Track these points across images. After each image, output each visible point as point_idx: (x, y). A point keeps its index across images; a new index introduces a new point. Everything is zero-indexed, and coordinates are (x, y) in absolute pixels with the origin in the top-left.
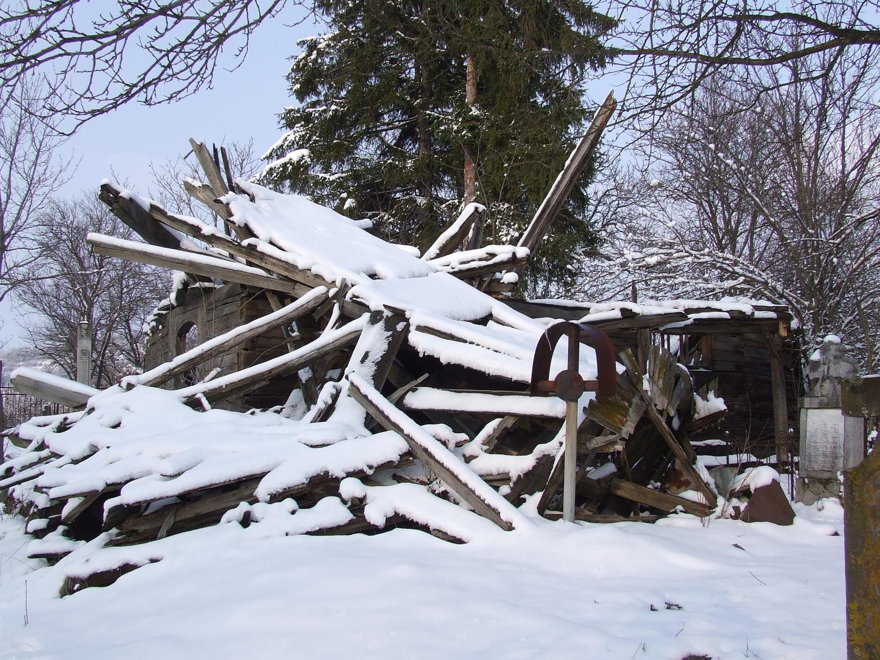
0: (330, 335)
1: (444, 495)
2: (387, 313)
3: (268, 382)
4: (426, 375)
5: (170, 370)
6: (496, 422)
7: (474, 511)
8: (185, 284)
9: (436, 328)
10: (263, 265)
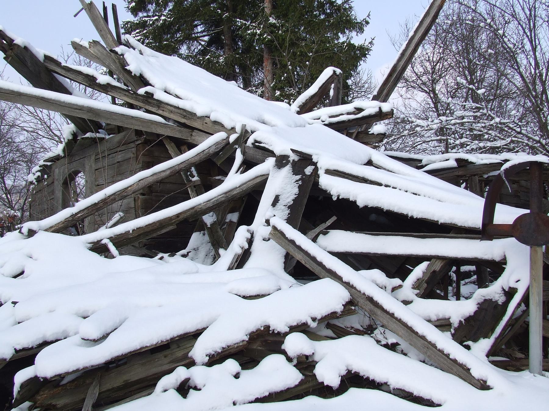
0: (234, 180)
1: (393, 347)
2: (293, 157)
3: (175, 227)
4: (334, 218)
5: (73, 216)
6: (424, 266)
7: (424, 362)
8: (75, 135)
9: (347, 172)
10: (160, 112)
